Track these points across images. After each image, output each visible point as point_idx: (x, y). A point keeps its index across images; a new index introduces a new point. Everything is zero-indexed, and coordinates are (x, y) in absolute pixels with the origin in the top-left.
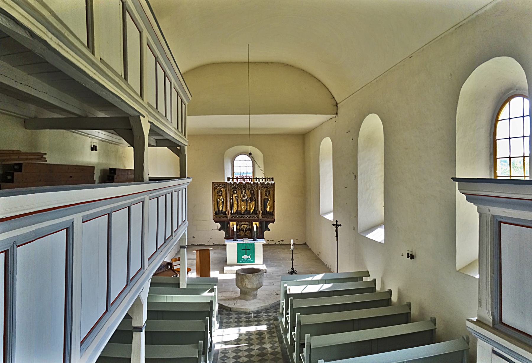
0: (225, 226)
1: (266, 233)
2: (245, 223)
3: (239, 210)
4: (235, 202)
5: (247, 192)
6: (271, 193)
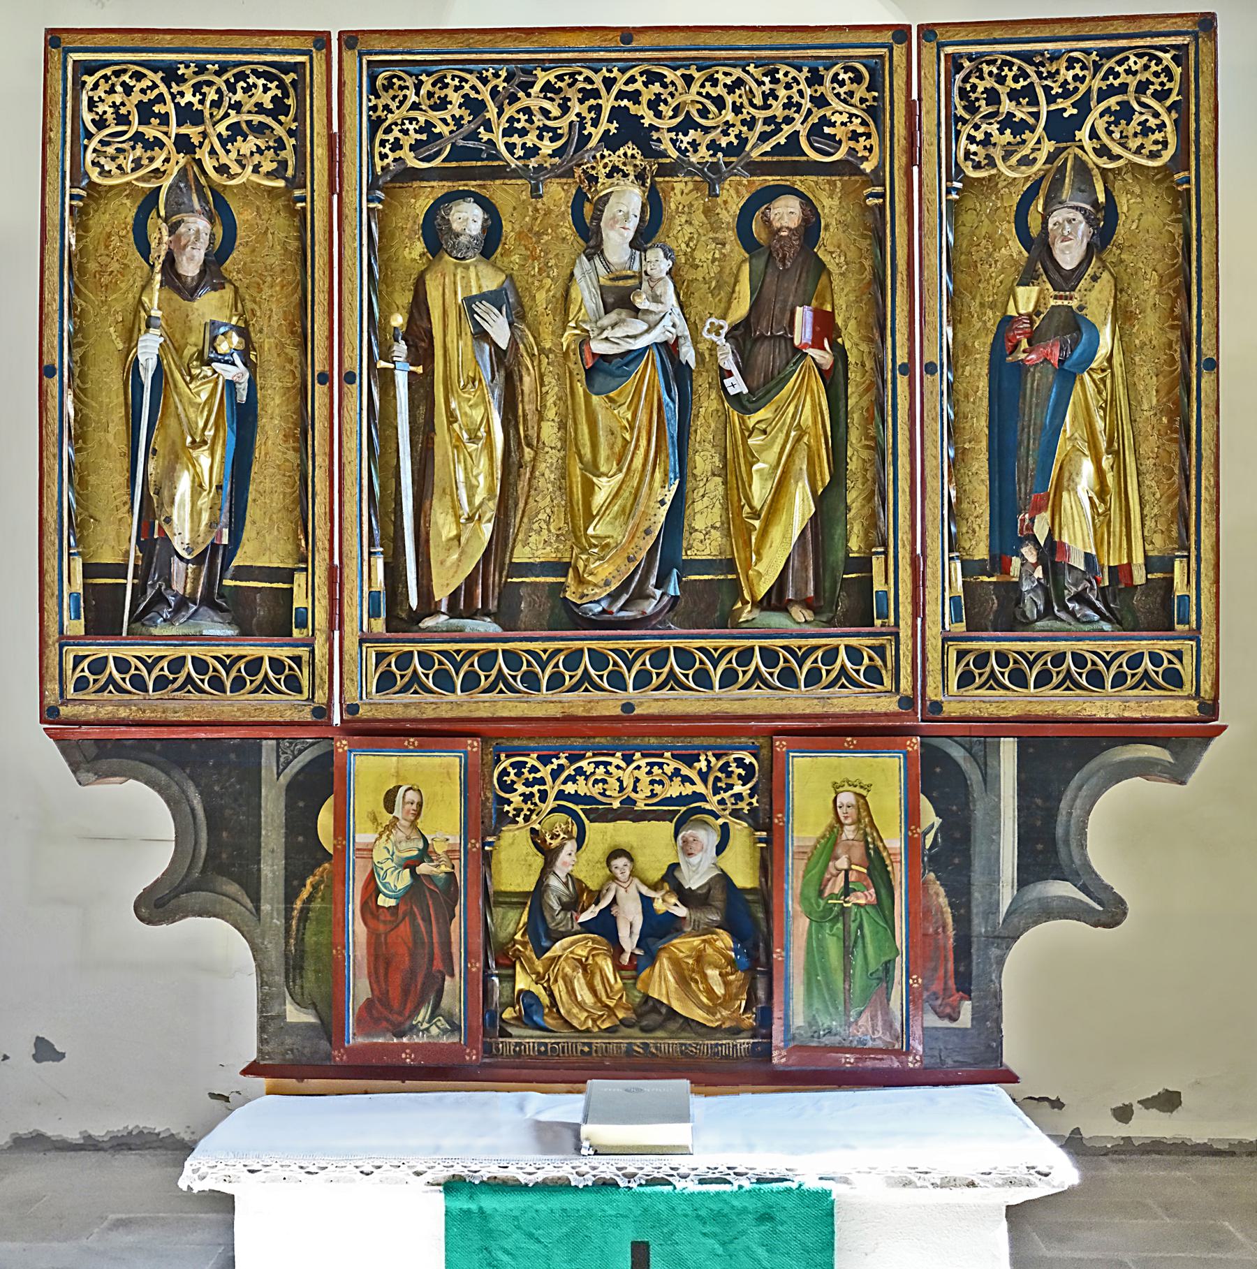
0: (244, 824)
1: (1038, 965)
2: (629, 776)
3: (532, 548)
4: (474, 409)
5: (681, 230)
6: (1141, 214)
